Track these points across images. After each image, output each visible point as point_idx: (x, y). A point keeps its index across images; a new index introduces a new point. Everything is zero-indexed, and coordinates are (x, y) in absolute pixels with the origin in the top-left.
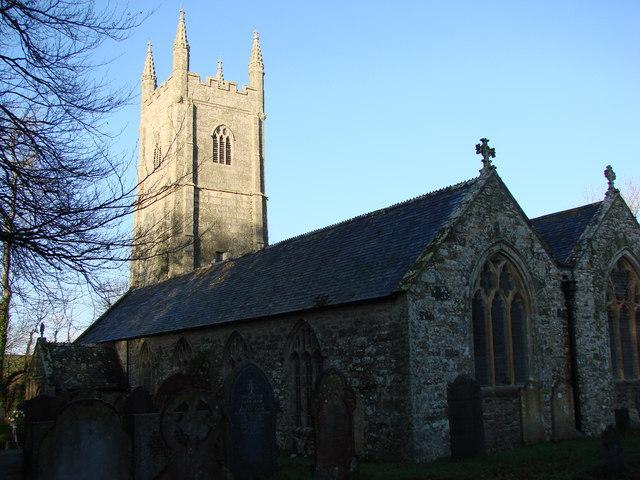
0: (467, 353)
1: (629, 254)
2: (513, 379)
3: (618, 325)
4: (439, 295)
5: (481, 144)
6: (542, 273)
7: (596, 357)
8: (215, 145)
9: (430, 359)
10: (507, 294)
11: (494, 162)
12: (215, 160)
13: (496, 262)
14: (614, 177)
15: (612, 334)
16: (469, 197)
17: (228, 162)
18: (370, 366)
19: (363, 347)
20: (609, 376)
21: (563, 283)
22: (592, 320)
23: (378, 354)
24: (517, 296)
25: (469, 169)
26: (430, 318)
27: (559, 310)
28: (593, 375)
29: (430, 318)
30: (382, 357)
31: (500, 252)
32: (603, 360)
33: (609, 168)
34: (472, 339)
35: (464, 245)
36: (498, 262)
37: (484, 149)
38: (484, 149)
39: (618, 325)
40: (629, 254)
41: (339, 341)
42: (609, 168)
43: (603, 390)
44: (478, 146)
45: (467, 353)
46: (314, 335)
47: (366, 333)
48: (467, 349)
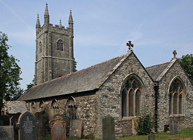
0: (119, 107)
1: (179, 78)
2: (135, 115)
3: (173, 99)
4: (110, 90)
5: (129, 43)
6: (147, 83)
7: (164, 108)
8: (58, 45)
9: (107, 109)
10: (128, 89)
11: (132, 48)
12: (58, 49)
13: (131, 80)
14: (176, 54)
15: (170, 101)
16: (123, 60)
17: (62, 50)
18: (88, 110)
19: (86, 105)
20: (168, 114)
21: (154, 86)
22: (164, 98)
23: (90, 107)
24: (138, 90)
25: (124, 51)
26: (106, 97)
27: (152, 95)
28: (163, 114)
29: (106, 97)
30: (91, 108)
31: (133, 77)
32: (166, 109)
33: (175, 51)
34: (121, 103)
35: (120, 75)
36: (133, 80)
37: (130, 44)
38: (130, 44)
39: (173, 99)
40: (179, 78)
41: (80, 103)
42: (175, 51)
43: (166, 118)
44: (127, 44)
45: (119, 107)
46: (74, 101)
47: (87, 101)
48: (119, 106)
